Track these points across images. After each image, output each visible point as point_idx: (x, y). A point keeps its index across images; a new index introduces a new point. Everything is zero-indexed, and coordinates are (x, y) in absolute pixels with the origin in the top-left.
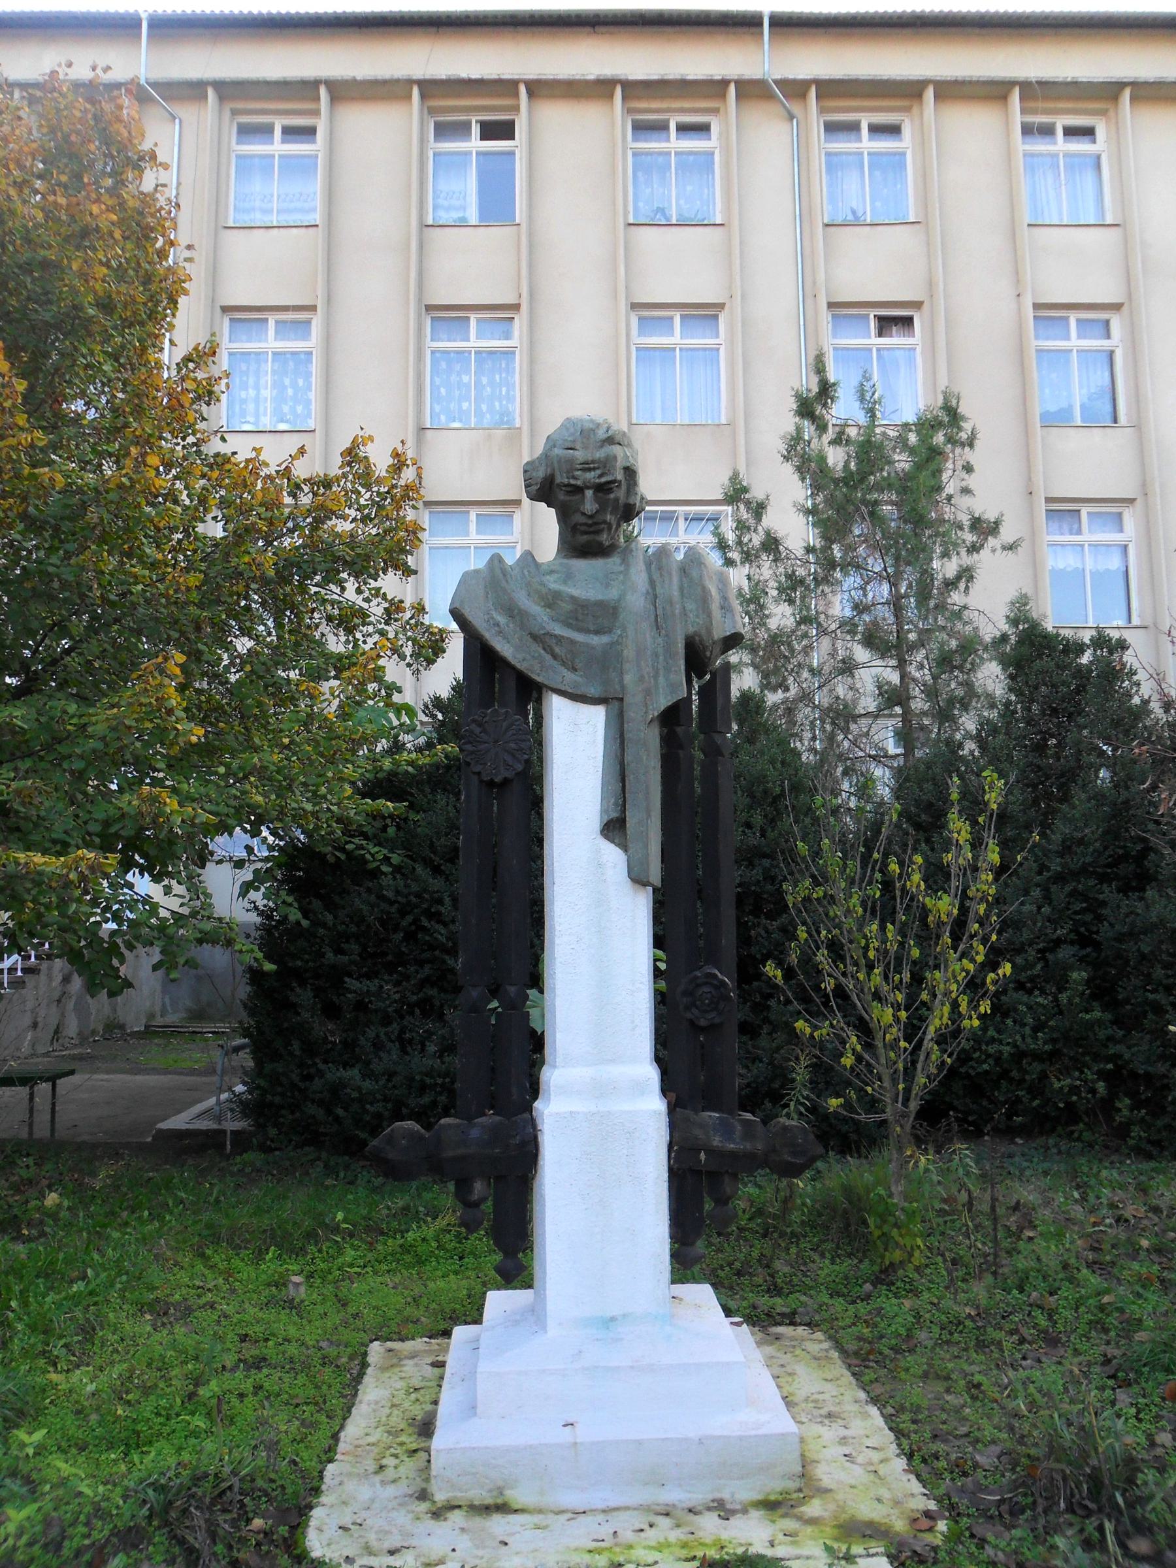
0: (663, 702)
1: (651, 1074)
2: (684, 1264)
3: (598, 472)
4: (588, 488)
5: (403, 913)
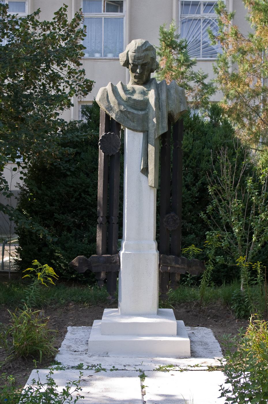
0: (161, 132)
1: (154, 245)
2: (164, 302)
3: (142, 60)
4: (139, 65)
5: (75, 191)
